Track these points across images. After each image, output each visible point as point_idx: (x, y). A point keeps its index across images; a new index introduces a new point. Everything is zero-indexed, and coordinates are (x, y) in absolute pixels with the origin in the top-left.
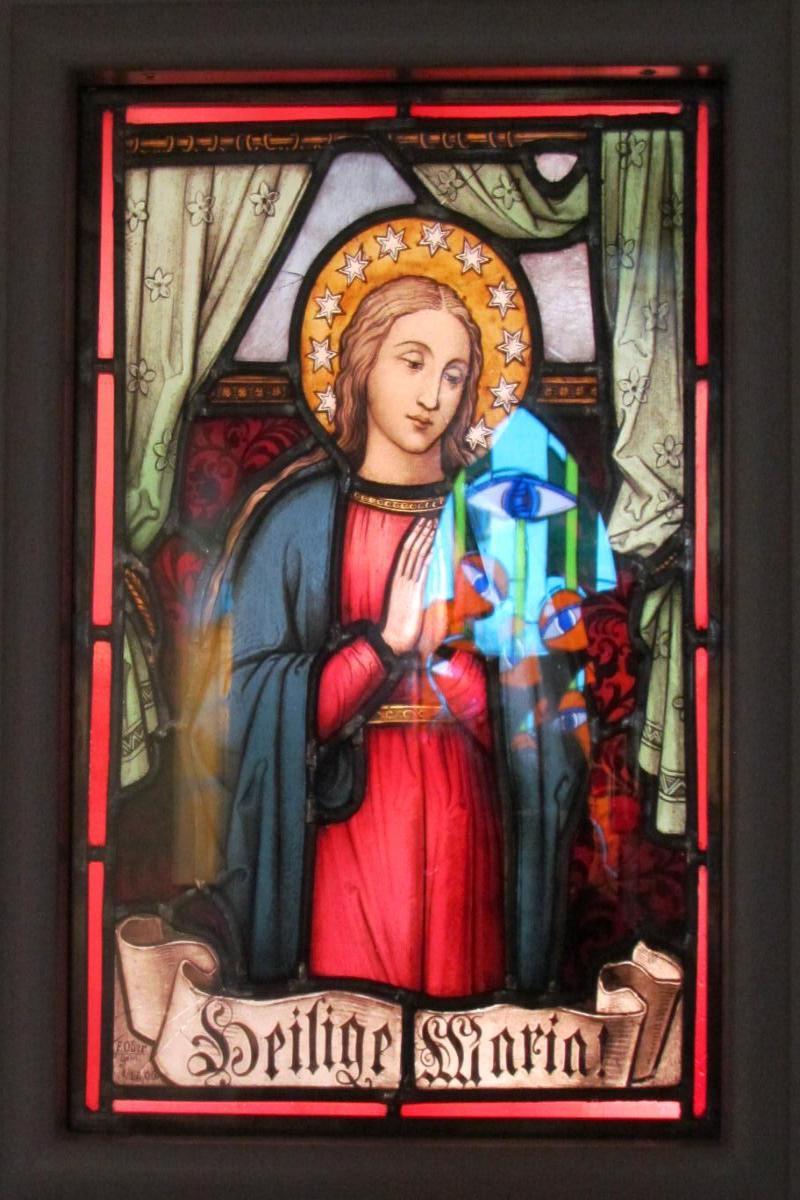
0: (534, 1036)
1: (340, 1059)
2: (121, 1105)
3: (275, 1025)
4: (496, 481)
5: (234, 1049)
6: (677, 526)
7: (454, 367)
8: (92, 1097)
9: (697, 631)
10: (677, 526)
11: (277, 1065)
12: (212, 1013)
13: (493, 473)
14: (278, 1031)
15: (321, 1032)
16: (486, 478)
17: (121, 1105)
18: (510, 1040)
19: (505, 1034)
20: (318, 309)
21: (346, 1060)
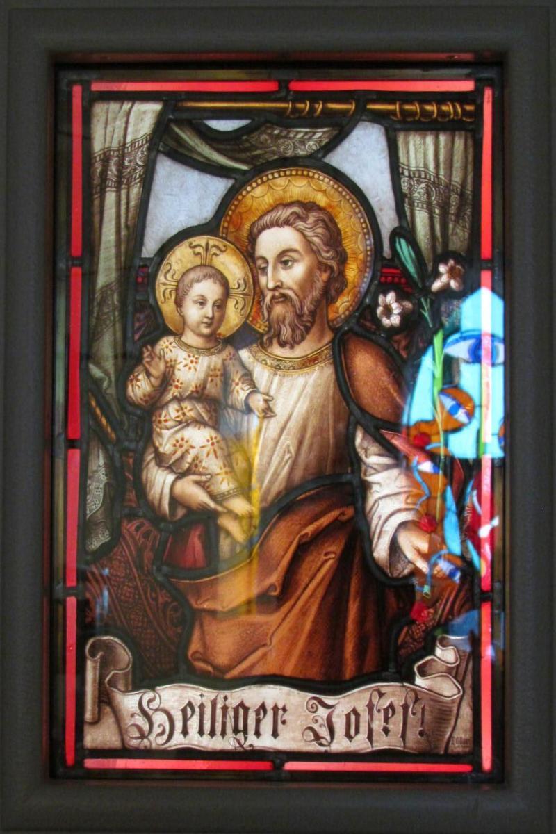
0: (281, 712)
1: (208, 732)
2: (90, 763)
3: (261, 703)
4: (464, 338)
5: (159, 726)
6: (150, 247)
7: (286, 256)
8: (70, 758)
9: (288, 343)
10: (150, 247)
11: (262, 731)
12: (148, 699)
13: (462, 333)
14: (263, 707)
15: (219, 712)
16: (456, 336)
17: (90, 763)
18: (357, 715)
19: (354, 711)
20: (214, 256)
21: (236, 731)
